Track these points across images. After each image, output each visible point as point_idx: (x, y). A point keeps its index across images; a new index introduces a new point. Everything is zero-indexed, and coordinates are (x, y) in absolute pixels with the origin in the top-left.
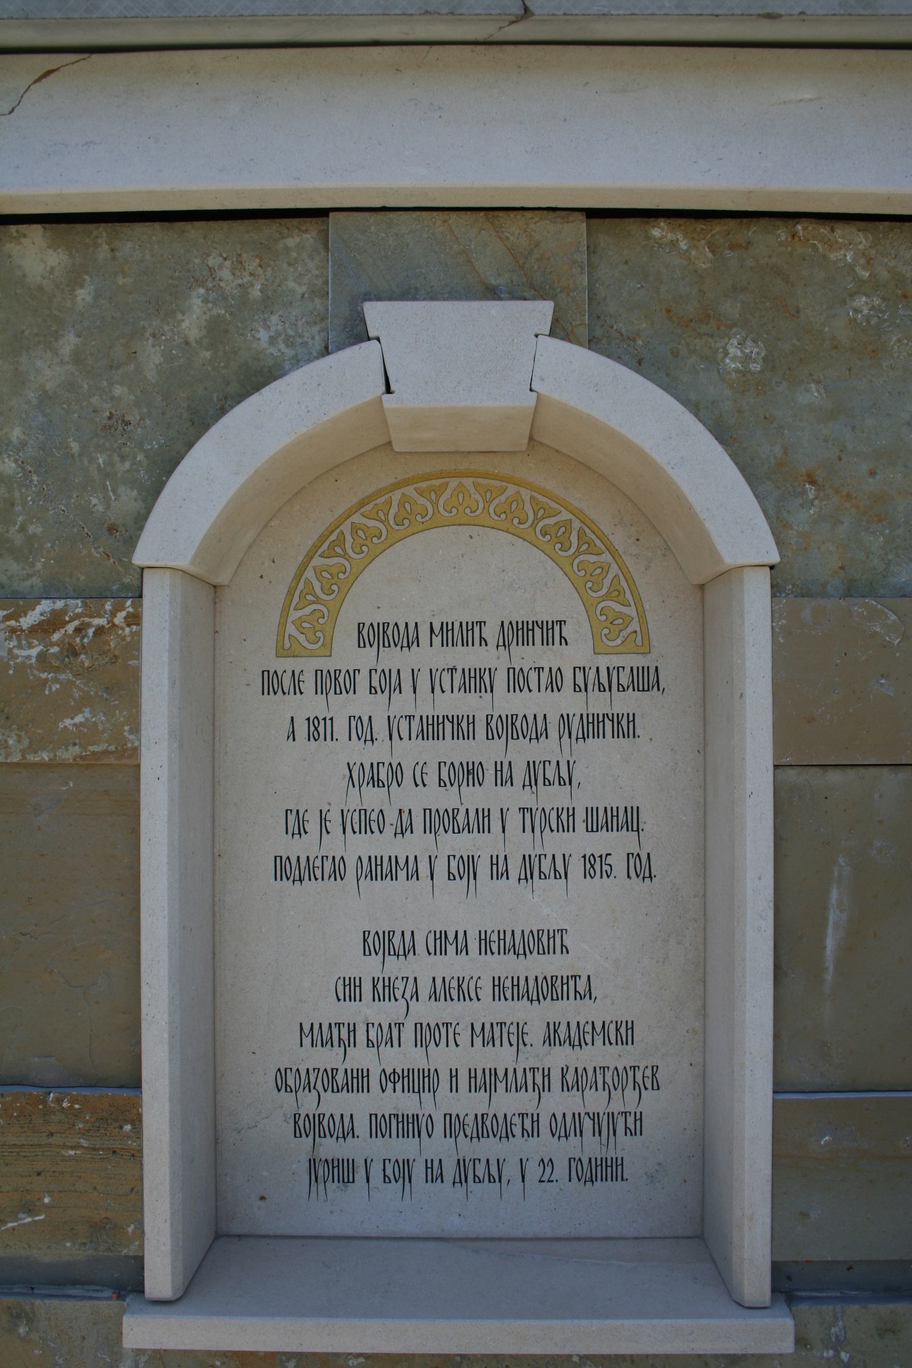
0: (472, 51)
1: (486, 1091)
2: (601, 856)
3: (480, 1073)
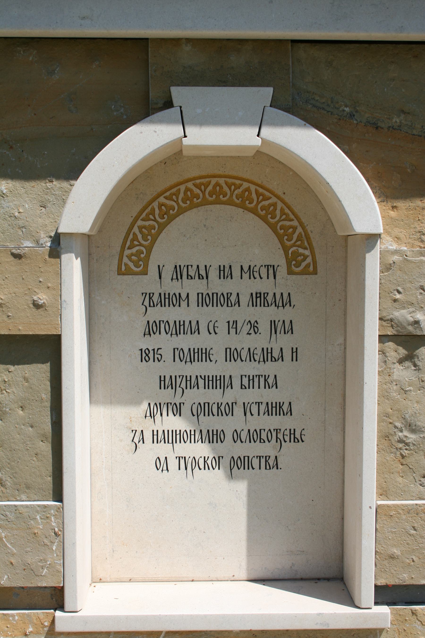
0: (117, 253)
1: (172, 388)
2: (154, 350)
3: (160, 433)
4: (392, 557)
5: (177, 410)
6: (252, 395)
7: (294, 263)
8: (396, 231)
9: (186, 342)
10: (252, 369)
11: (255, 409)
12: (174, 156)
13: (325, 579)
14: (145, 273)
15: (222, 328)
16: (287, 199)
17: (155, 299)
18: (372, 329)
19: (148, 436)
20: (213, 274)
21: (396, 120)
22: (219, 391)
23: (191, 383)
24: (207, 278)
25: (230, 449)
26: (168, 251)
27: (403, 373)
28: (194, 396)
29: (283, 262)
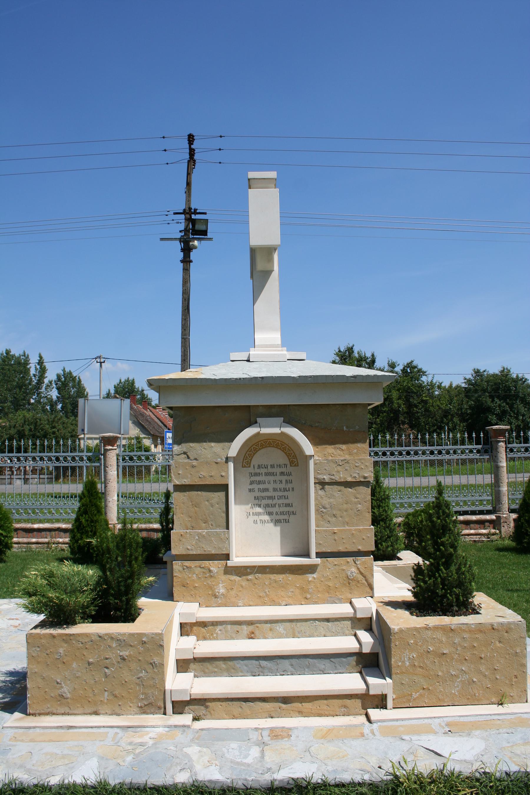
4: (320, 544)
5: (260, 506)
6: (281, 501)
7: (292, 463)
8: (318, 454)
9: (262, 486)
10: (281, 494)
11: (282, 505)
12: (258, 434)
13: (186, 271)
14: (250, 467)
15: (272, 482)
16: (289, 445)
17: (253, 474)
18: (312, 481)
19: (251, 514)
20: (269, 467)
21: (317, 424)
22: (271, 500)
23: (263, 498)
25: (275, 517)
26: (256, 460)
27: (321, 493)
28: (264, 502)
29: (289, 463)
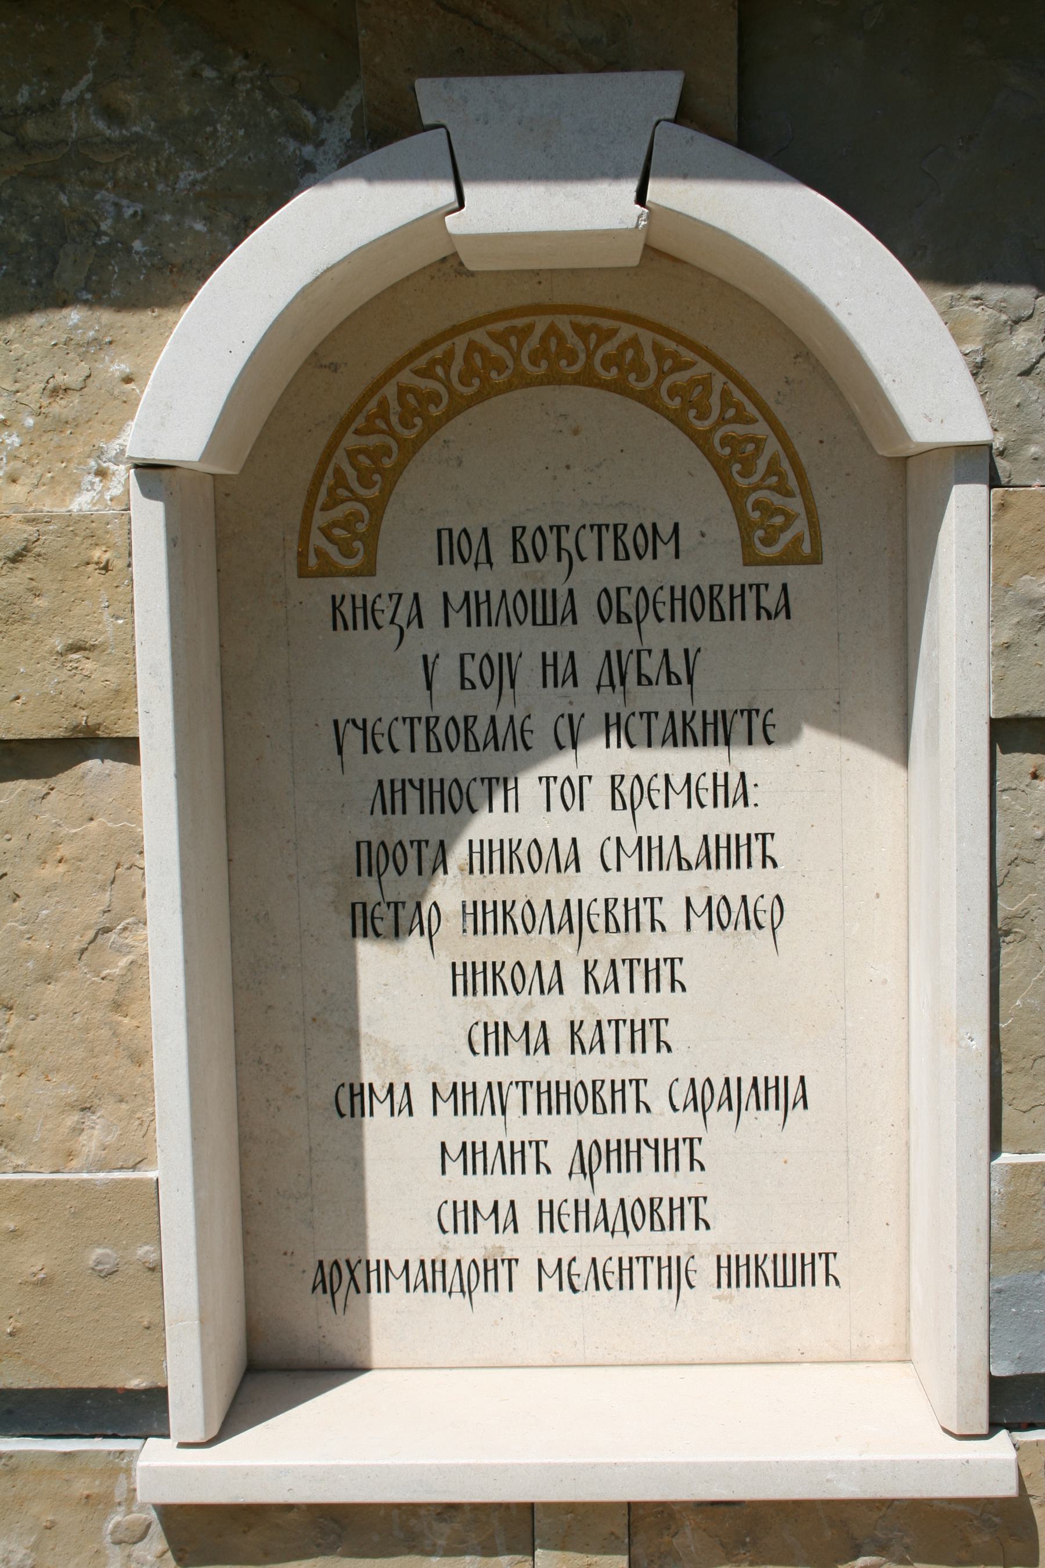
1: (730, 1108)
24: (690, 680)
